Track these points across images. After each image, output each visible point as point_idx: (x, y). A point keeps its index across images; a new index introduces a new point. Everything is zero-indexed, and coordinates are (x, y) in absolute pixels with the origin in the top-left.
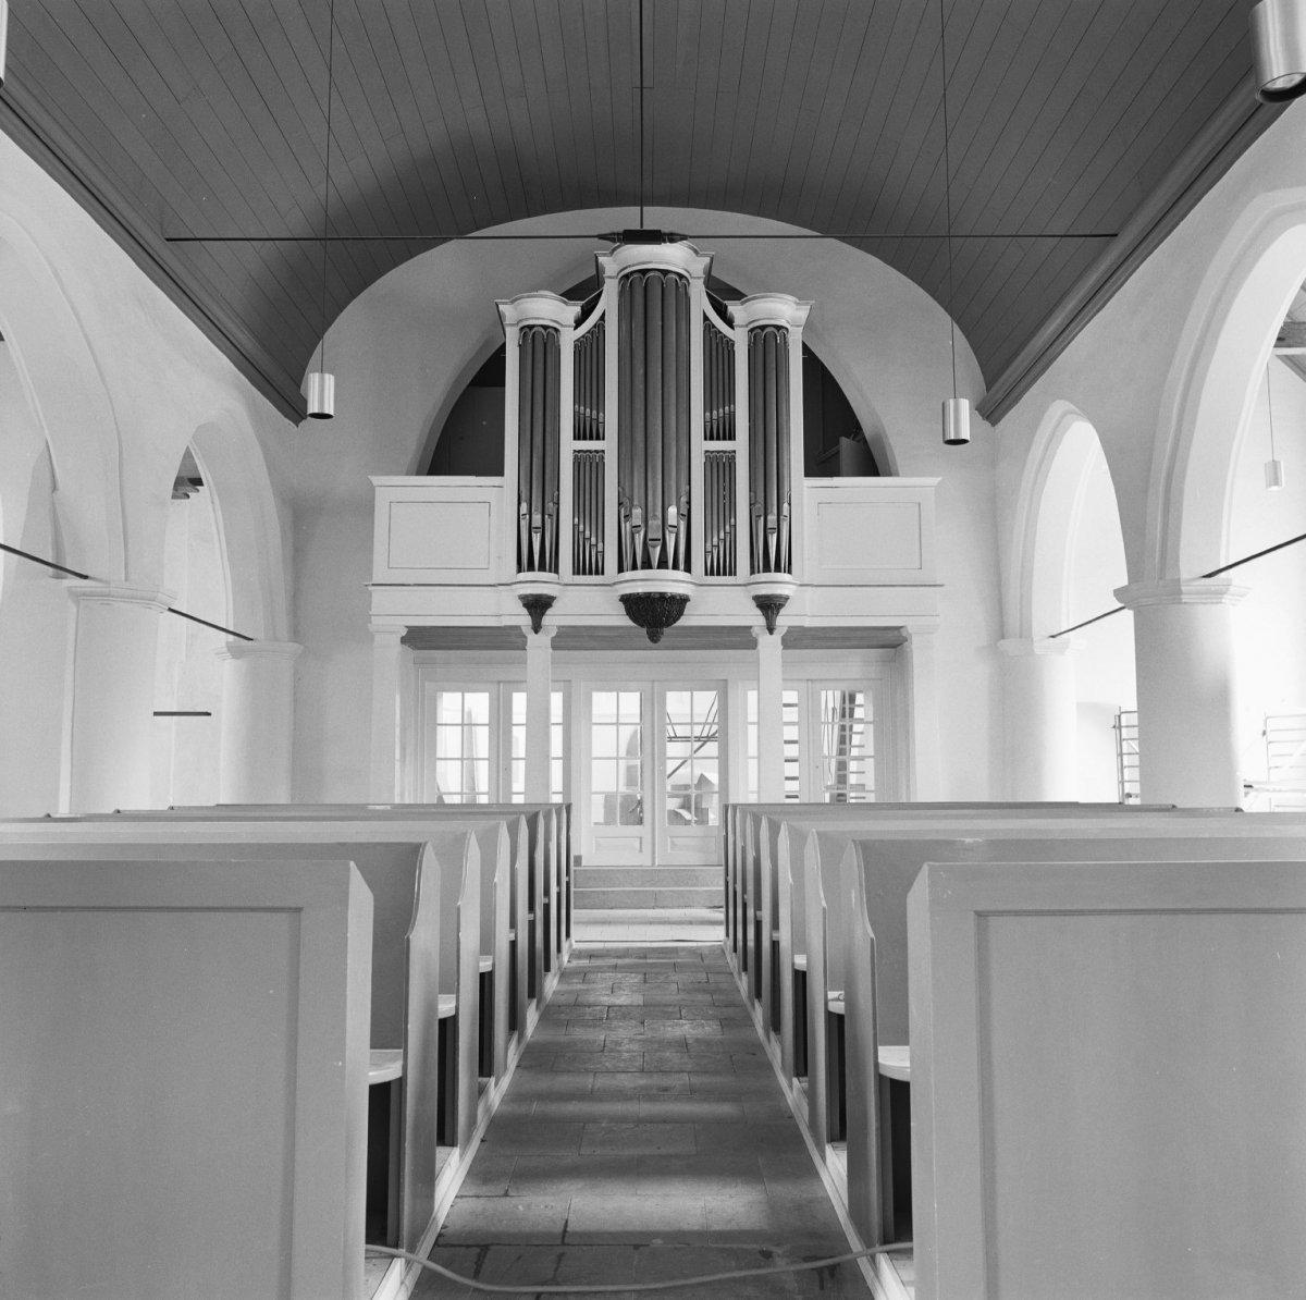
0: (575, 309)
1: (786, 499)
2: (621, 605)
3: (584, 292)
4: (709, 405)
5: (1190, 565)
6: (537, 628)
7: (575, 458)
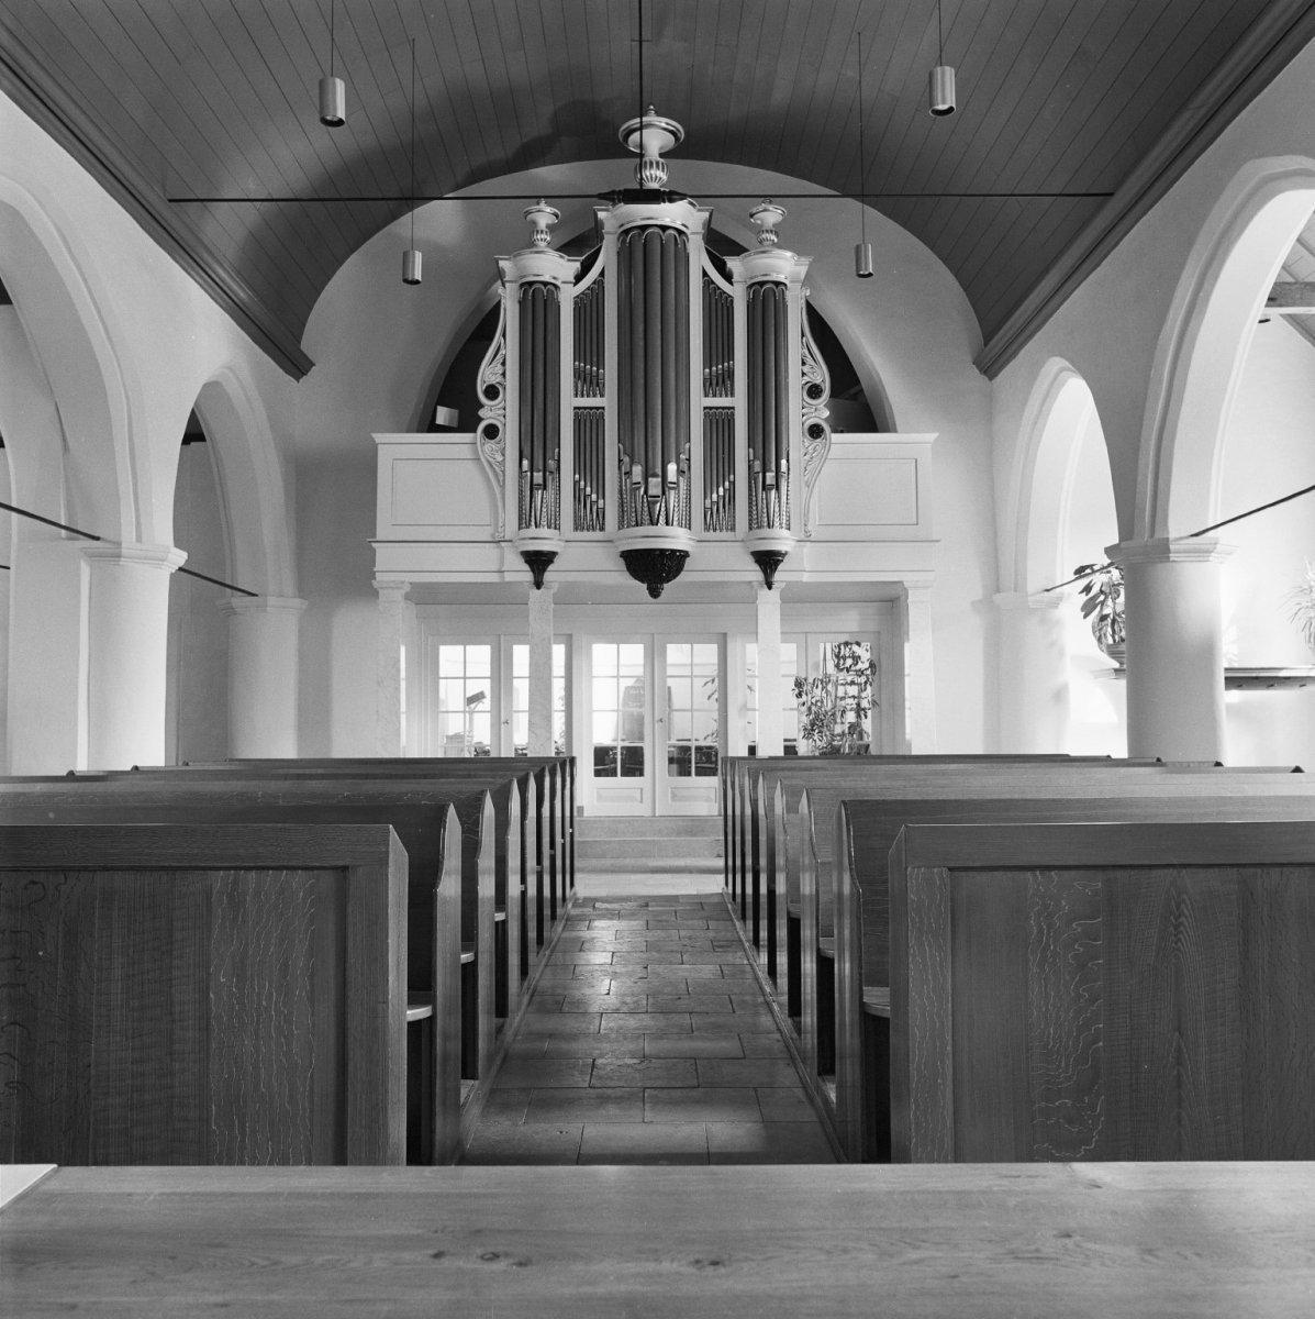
0: (574, 266)
1: (784, 455)
2: (622, 561)
3: (580, 244)
4: (708, 361)
5: (1178, 525)
6: (538, 584)
7: (576, 415)
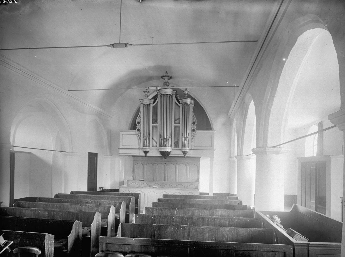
5: (270, 142)
